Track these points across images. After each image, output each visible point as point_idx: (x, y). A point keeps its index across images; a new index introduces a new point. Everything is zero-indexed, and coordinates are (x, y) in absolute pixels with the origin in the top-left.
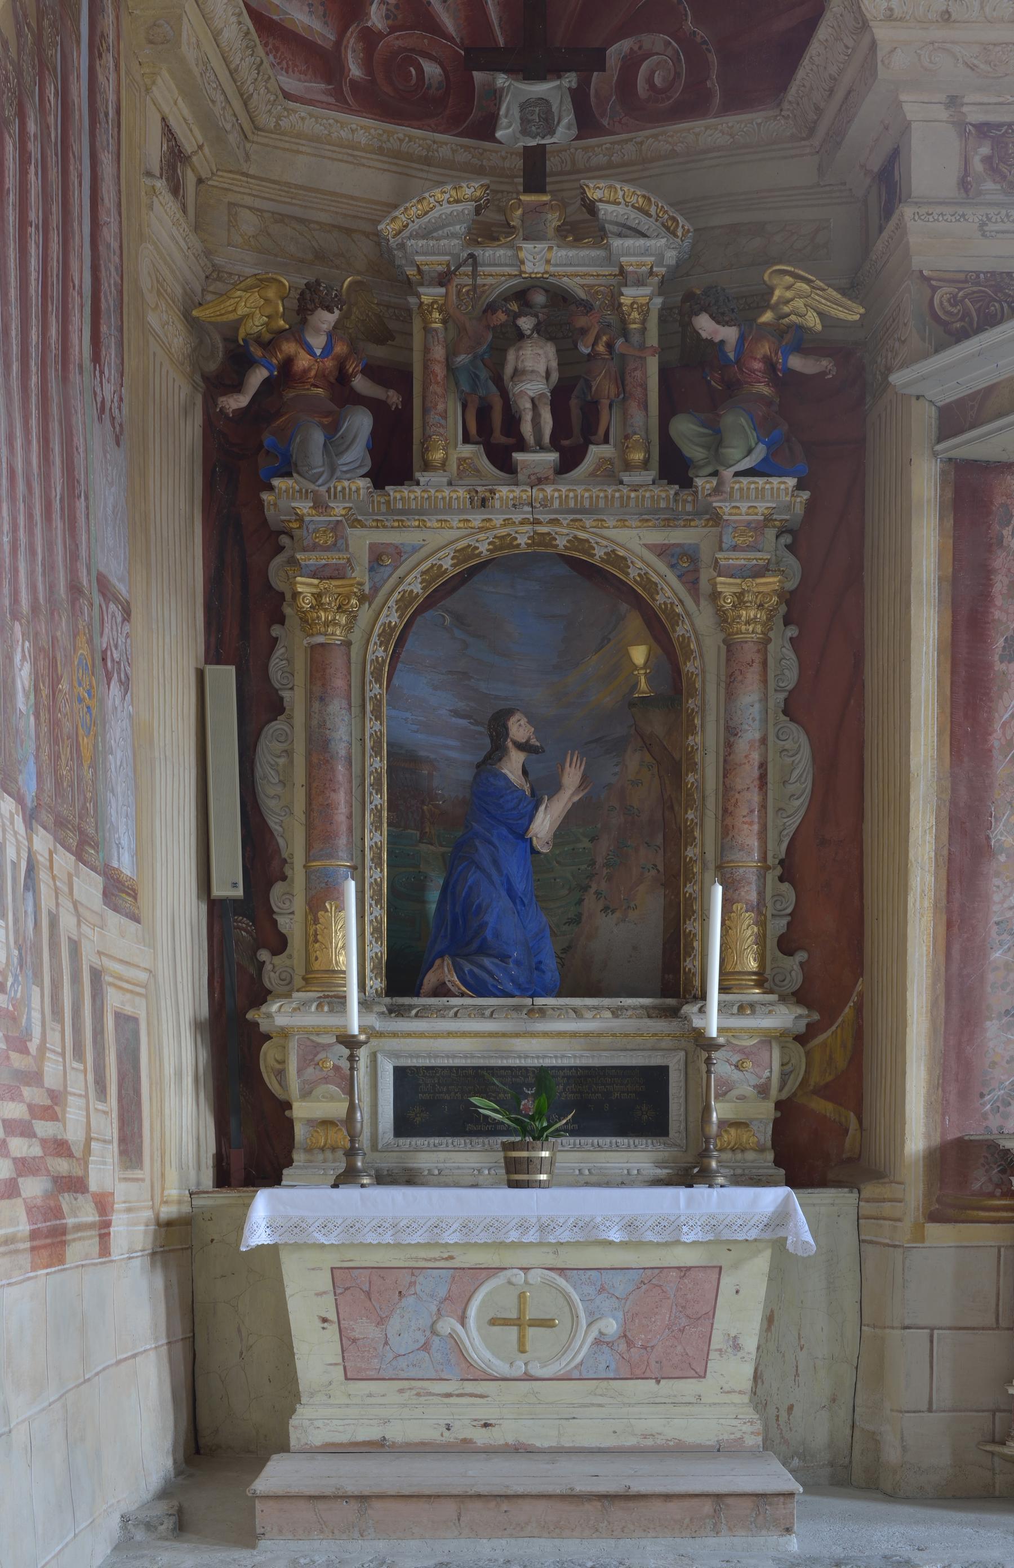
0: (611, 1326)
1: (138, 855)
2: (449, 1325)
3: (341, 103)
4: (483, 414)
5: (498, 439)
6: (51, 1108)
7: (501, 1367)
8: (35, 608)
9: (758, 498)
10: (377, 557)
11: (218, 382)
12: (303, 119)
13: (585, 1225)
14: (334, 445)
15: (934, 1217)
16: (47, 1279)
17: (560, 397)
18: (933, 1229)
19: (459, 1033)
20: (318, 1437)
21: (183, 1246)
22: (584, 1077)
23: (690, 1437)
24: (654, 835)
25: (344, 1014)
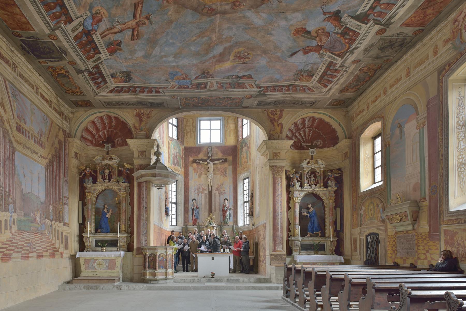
0: (107, 265)
1: (69, 221)
2: (94, 265)
3: (93, 146)
4: (103, 176)
5: (104, 180)
6: (54, 244)
7: (98, 269)
8: (53, 203)
11: (81, 174)
12: (89, 147)
13: (104, 255)
14: (89, 180)
15: (137, 255)
16: (53, 259)
17: (109, 175)
18: (137, 256)
19: (101, 236)
20: (83, 276)
21: (73, 257)
22: (111, 241)
24: (117, 217)
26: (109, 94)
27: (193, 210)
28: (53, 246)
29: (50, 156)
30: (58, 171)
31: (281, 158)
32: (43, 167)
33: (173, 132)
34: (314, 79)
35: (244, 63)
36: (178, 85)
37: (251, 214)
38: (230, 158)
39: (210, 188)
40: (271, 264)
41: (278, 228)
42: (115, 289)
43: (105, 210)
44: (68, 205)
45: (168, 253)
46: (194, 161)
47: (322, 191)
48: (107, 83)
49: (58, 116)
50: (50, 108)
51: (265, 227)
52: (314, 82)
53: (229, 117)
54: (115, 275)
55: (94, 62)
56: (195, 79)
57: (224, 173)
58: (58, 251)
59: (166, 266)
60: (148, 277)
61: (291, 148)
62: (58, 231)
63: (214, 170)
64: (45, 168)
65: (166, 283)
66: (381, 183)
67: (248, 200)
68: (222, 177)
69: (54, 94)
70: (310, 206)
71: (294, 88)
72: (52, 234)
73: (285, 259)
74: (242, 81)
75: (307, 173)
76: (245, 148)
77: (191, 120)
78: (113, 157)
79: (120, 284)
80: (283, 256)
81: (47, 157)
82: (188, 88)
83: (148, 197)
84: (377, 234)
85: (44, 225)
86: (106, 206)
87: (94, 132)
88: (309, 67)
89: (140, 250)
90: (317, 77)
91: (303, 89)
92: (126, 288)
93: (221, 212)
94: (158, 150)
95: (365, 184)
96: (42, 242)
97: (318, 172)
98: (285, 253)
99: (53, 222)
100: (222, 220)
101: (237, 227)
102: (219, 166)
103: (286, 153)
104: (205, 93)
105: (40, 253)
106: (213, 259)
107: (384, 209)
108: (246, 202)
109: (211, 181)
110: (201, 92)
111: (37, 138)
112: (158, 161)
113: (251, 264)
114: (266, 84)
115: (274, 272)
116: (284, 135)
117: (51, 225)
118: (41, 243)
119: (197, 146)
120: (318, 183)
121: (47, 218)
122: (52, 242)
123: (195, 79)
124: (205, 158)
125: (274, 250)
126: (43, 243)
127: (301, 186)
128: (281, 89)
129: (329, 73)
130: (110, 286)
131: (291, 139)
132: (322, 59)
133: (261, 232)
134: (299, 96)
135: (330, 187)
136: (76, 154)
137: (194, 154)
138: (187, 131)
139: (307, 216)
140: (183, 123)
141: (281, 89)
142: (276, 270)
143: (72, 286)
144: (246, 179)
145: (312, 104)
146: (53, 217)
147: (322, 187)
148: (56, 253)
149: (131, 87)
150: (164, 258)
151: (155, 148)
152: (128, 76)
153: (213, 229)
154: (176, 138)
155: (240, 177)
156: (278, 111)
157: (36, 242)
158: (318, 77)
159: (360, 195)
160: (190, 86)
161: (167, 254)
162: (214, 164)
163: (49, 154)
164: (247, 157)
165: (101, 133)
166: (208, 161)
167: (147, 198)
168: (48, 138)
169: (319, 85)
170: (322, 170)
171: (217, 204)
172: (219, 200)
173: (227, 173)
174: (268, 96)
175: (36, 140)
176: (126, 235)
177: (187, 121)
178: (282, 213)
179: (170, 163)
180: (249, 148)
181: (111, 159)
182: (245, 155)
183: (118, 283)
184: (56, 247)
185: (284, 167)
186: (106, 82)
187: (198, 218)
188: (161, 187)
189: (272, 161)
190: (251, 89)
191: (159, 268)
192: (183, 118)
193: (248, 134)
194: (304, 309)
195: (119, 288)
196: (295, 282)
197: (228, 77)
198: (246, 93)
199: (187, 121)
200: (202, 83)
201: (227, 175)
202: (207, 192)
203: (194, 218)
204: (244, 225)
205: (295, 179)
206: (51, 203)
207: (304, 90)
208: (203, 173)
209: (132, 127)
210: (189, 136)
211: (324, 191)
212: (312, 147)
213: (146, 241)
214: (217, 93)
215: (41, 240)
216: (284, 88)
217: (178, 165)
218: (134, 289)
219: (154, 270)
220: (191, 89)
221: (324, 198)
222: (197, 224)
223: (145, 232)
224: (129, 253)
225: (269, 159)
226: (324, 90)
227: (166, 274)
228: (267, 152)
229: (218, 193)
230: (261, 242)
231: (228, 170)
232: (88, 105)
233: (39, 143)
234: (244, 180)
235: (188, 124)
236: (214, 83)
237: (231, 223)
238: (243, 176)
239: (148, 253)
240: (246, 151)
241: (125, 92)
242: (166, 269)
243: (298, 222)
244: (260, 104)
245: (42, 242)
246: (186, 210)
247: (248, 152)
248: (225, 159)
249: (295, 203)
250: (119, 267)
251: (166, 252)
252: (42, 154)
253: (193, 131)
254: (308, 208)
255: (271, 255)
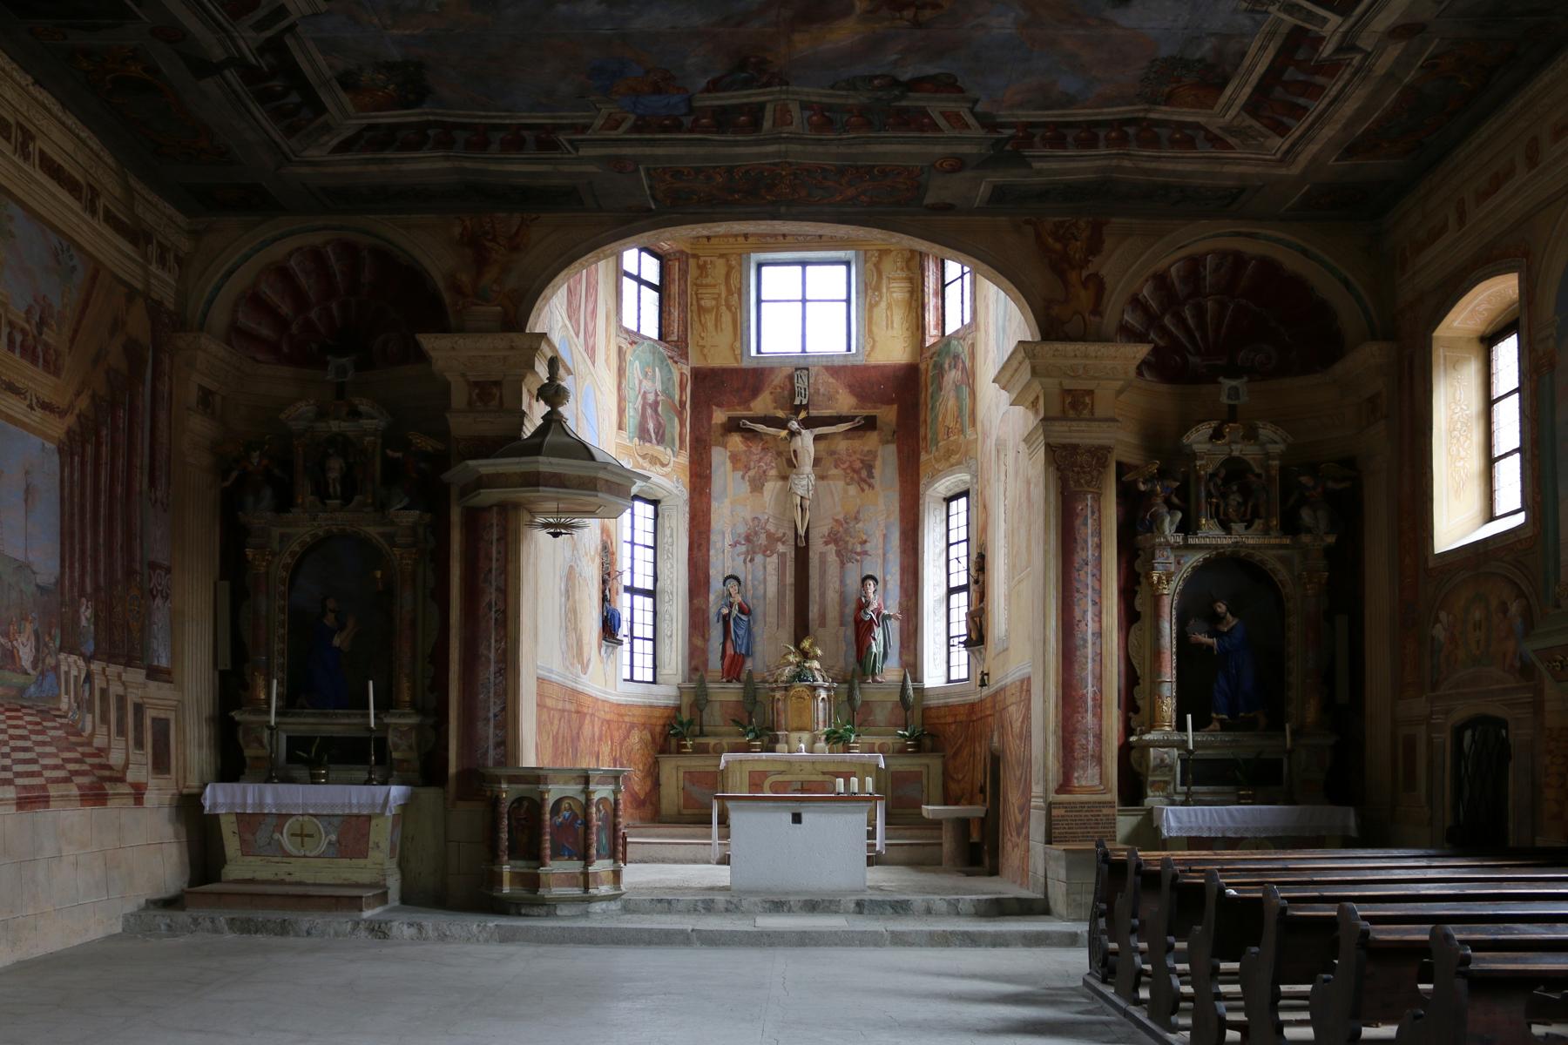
2: (277, 836)
5: (322, 492)
7: (294, 851)
8: (97, 588)
9: (408, 518)
10: (282, 536)
20: (232, 876)
23: (360, 881)
25: (271, 716)
26: (337, 157)
27: (725, 619)
28: (96, 761)
29: (83, 403)
30: (120, 462)
31: (1099, 413)
32: (50, 446)
33: (642, 311)
34: (1231, 101)
35: (917, 24)
36: (632, 117)
37: (976, 638)
38: (888, 414)
39: (802, 532)
40: (1049, 840)
41: (1084, 697)
42: (363, 934)
43: (330, 620)
44: (166, 598)
45: (596, 797)
46: (733, 426)
47: (1273, 547)
48: (324, 110)
49: (127, 247)
50: (87, 217)
51: (1029, 691)
52: (1232, 112)
53: (883, 253)
54: (365, 877)
55: (260, 26)
56: (707, 90)
57: (862, 474)
58: (122, 780)
59: (587, 847)
60: (506, 890)
61: (1140, 373)
62: (121, 700)
63: (817, 462)
64: (60, 451)
65: (586, 914)
66: (1520, 519)
67: (963, 581)
68: (853, 490)
69: (110, 161)
70: (1221, 608)
71: (1148, 134)
72: (91, 710)
73: (1112, 823)
74: (913, 100)
75: (1213, 476)
76: (952, 376)
77: (720, 263)
78: (362, 408)
79: (387, 917)
80: (1105, 811)
81: (71, 406)
82: (678, 127)
83: (510, 567)
84: (1501, 723)
85: (51, 676)
86: (331, 604)
87: (286, 309)
88: (1206, 49)
89: (476, 784)
90: (1239, 91)
91: (1186, 137)
92: (408, 932)
93: (850, 632)
94: (553, 375)
95: (1456, 522)
96: (44, 744)
97: (1257, 470)
98: (1113, 796)
99: (96, 666)
100: (852, 659)
101: (920, 691)
102: (842, 445)
103: (1120, 392)
104: (755, 150)
105: (33, 787)
106: (797, 818)
107: (1529, 621)
108: (959, 589)
109: (807, 503)
110: (736, 143)
111: (23, 331)
112: (553, 420)
113: (975, 838)
114: (1020, 112)
115: (1062, 873)
116: (1110, 320)
117: (89, 677)
118: (38, 749)
119: (745, 364)
120: (1256, 514)
121: (69, 647)
122: (90, 744)
123: (707, 90)
124: (780, 414)
125: (1065, 786)
126: (48, 749)
127: (1186, 527)
128: (1089, 134)
129: (1290, 74)
130: (340, 922)
131: (1140, 338)
132: (1258, 17)
133: (1014, 712)
134: (1169, 166)
135: (1309, 531)
136: (206, 396)
137: (727, 402)
138: (698, 300)
139: (1210, 648)
140: (684, 273)
141: (1089, 134)
142: (1069, 869)
143: (182, 917)
144: (956, 497)
145: (1227, 201)
146: (97, 645)
147: (1273, 533)
148: (109, 788)
149: (429, 124)
150: (575, 817)
151: (542, 371)
152: (411, 82)
153: (815, 698)
154: (655, 336)
155: (930, 492)
156: (1082, 224)
157: (12, 743)
158: (1248, 90)
159: (1431, 565)
160: (688, 121)
161: (588, 800)
162: (817, 438)
163: (78, 394)
164: (960, 409)
165: (313, 315)
166: (794, 425)
167: (504, 571)
168: (76, 331)
169: (1254, 123)
170: (1276, 463)
171: (832, 596)
172: (842, 581)
173: (877, 472)
174: (1037, 165)
175: (18, 338)
176: (413, 720)
177: (702, 268)
178: (1099, 634)
179: (624, 434)
180: (970, 376)
181: (355, 414)
182: (951, 403)
183: (378, 910)
184: (111, 762)
185: (1109, 449)
186: (320, 109)
187: (749, 653)
188: (567, 526)
189: (1058, 427)
190: (956, 133)
191: (556, 855)
192: (682, 257)
193: (967, 320)
194: (1171, 1037)
195: (379, 931)
196: (1136, 922)
197: (851, 85)
198: (939, 149)
199: (702, 268)
200: (739, 109)
201: (876, 482)
202: (787, 549)
203: (730, 651)
204: (949, 681)
205: (1159, 500)
206: (89, 589)
207: (1189, 143)
208: (773, 472)
209: (441, 284)
210: (710, 325)
211: (1281, 546)
212: (1233, 373)
213: (502, 743)
214: (810, 148)
215: (40, 738)
216: (1102, 134)
217: (661, 439)
218: (443, 937)
219: (533, 864)
220: (691, 131)
221: (1282, 574)
222: (744, 676)
223: (493, 710)
224: (429, 794)
225: (1044, 420)
226: (1278, 144)
227: (586, 880)
228: (1037, 387)
229: (838, 553)
230: (1013, 747)
231: (878, 463)
232: (255, 201)
233: (29, 353)
234: (948, 500)
235: (709, 280)
236: (795, 109)
237: (891, 671)
238: (944, 486)
239: (507, 792)
240: (957, 388)
241: (407, 146)
242: (586, 859)
243: (1169, 673)
244: (1000, 196)
245: (44, 744)
246: (697, 621)
247: (966, 391)
248: (866, 418)
249: (1157, 599)
250: (385, 845)
251: (587, 793)
252: (47, 395)
253: (729, 307)
254: (1215, 619)
255: (1050, 807)
